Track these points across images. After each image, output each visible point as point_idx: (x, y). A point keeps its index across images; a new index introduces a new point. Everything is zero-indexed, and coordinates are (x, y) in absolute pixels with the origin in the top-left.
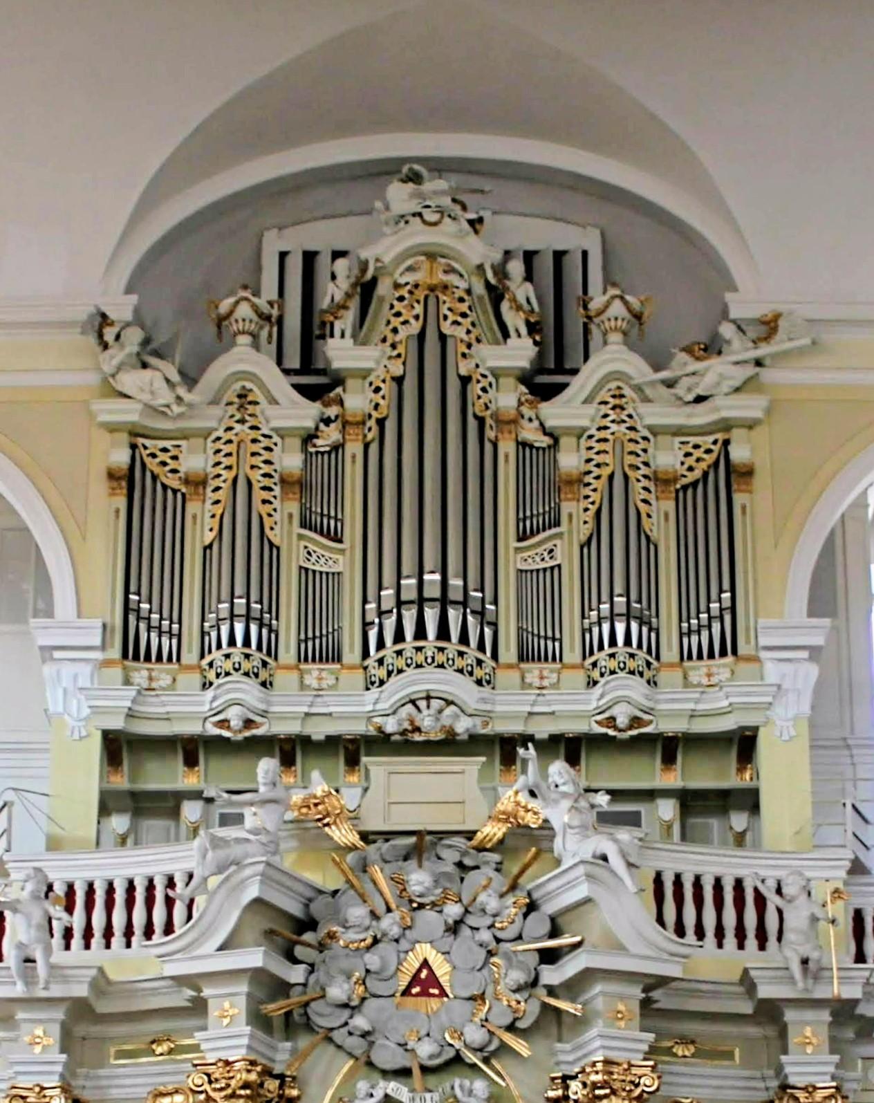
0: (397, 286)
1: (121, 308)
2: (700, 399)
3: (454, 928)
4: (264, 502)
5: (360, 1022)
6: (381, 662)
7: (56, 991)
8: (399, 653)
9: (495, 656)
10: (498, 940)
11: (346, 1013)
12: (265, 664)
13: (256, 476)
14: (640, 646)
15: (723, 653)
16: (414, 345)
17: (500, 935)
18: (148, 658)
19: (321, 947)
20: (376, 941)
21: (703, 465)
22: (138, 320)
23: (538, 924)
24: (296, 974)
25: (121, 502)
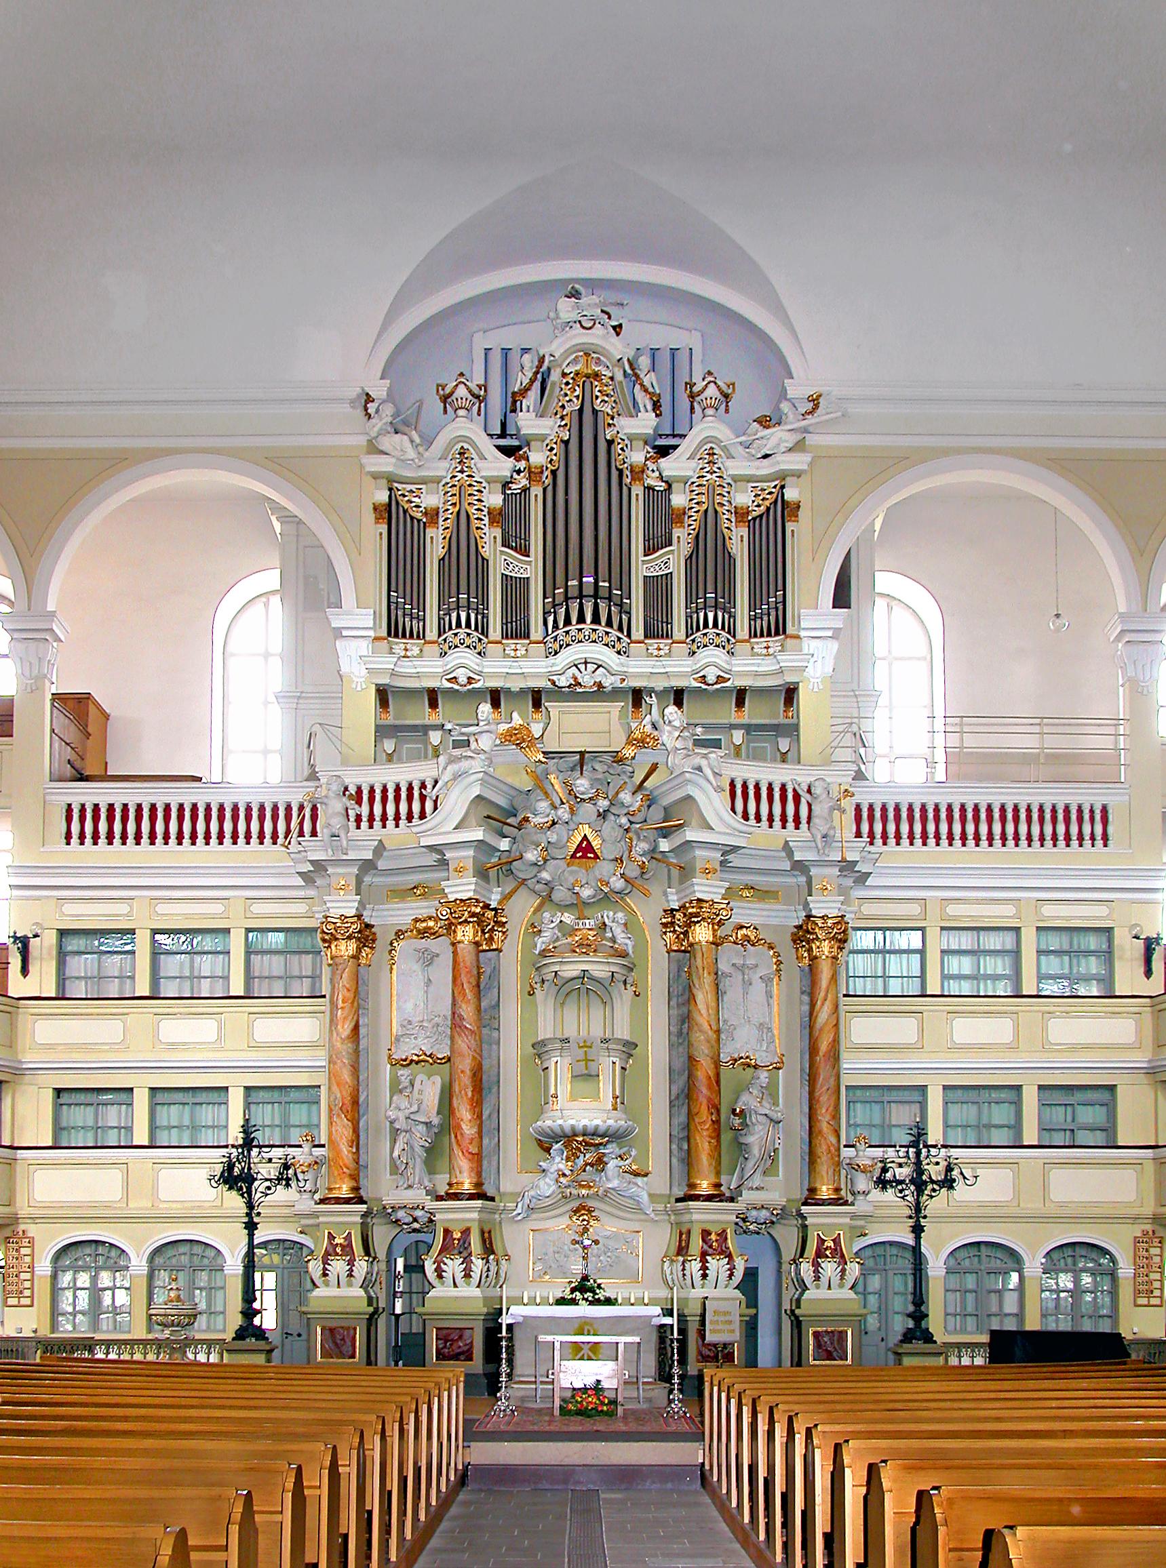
0: (564, 375)
1: (379, 390)
2: (766, 456)
3: (603, 815)
5: (545, 875)
6: (555, 638)
7: (352, 856)
8: (567, 632)
9: (629, 635)
10: (631, 823)
11: (536, 869)
12: (480, 640)
14: (723, 628)
15: (777, 634)
16: (576, 415)
17: (632, 819)
18: (404, 636)
19: (519, 828)
20: (554, 823)
21: (767, 503)
22: (390, 397)
23: (656, 814)
24: (504, 844)
25: (384, 528)
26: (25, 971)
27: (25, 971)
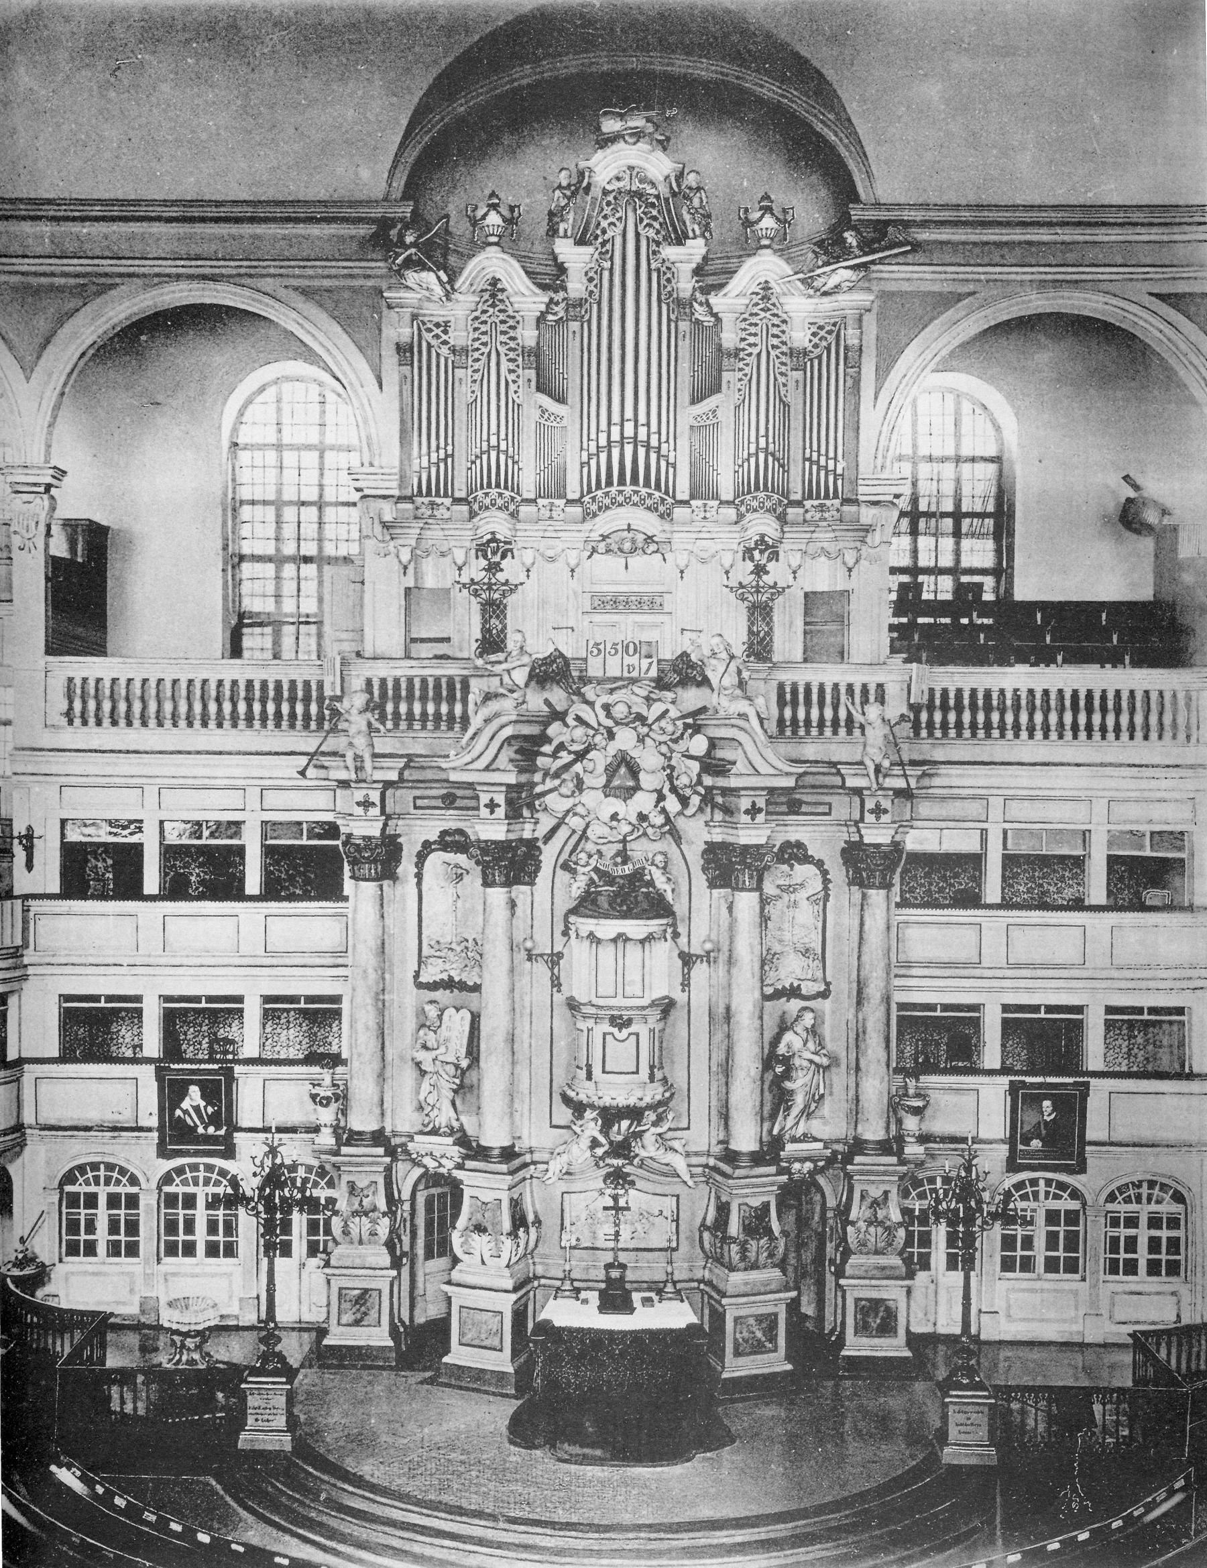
4: (511, 371)
13: (502, 350)
26: (29, 866)
27: (29, 866)
